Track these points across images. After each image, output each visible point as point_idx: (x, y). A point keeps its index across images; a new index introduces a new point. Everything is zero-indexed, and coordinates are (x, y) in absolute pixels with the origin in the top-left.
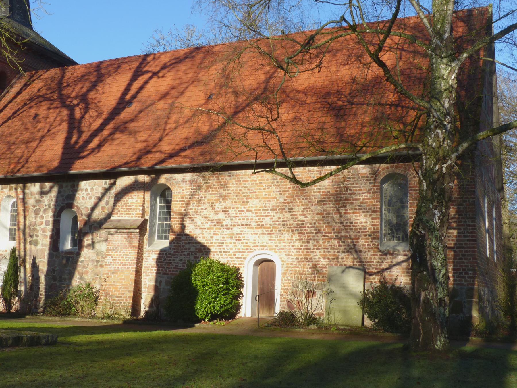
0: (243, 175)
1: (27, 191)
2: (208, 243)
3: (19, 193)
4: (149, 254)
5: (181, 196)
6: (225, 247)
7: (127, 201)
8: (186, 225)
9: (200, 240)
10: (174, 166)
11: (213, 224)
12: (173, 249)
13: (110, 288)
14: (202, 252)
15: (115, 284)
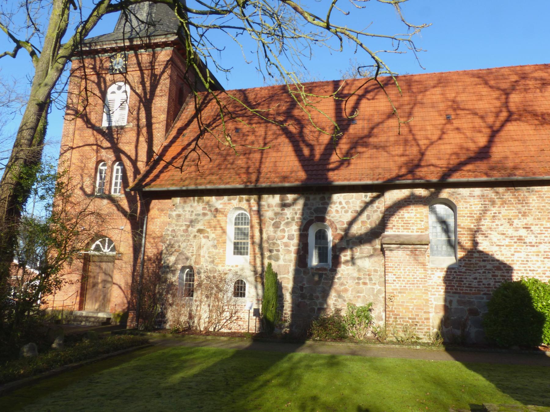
0: (546, 191)
1: (263, 203)
2: (509, 261)
3: (252, 205)
4: (432, 271)
5: (469, 211)
6: (531, 266)
7: (403, 215)
8: (478, 241)
9: (499, 256)
10: (464, 179)
11: (513, 241)
12: (464, 266)
13: (399, 309)
14: (502, 270)
15: (405, 304)
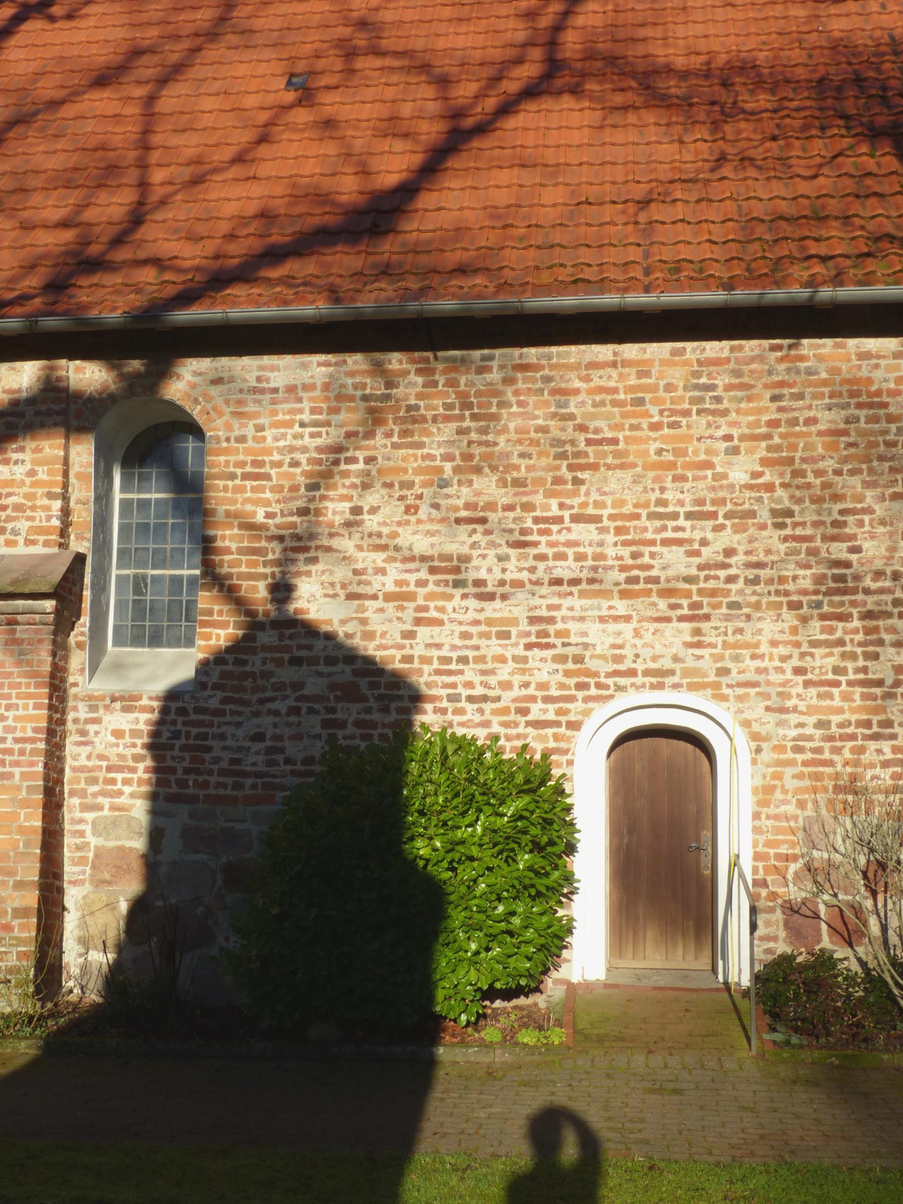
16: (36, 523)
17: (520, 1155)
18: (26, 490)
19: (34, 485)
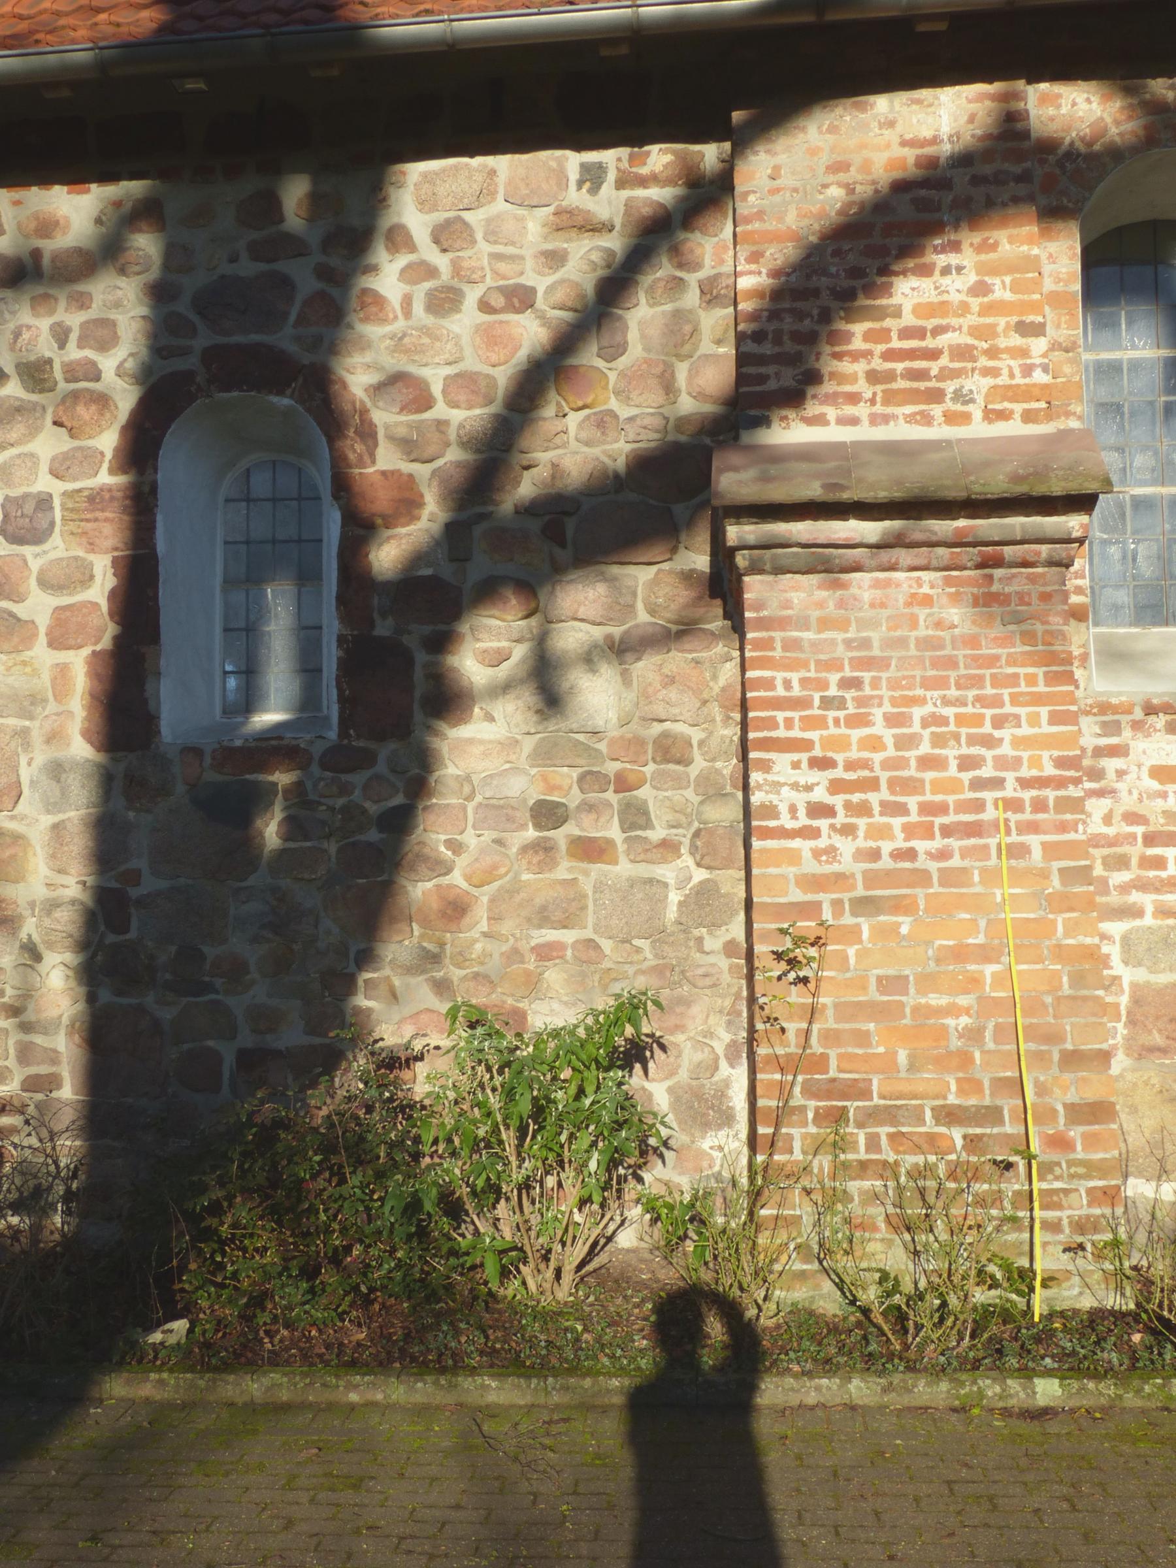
2: (1012, 661)
13: (863, 1038)
15: (911, 999)
16: (1003, 380)
17: (643, 1353)
18: (972, 319)
19: (986, 310)
